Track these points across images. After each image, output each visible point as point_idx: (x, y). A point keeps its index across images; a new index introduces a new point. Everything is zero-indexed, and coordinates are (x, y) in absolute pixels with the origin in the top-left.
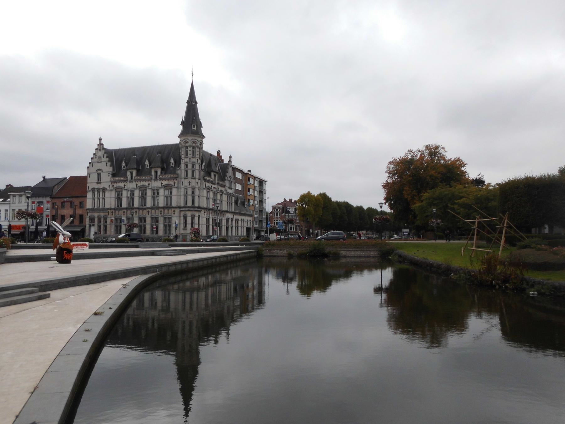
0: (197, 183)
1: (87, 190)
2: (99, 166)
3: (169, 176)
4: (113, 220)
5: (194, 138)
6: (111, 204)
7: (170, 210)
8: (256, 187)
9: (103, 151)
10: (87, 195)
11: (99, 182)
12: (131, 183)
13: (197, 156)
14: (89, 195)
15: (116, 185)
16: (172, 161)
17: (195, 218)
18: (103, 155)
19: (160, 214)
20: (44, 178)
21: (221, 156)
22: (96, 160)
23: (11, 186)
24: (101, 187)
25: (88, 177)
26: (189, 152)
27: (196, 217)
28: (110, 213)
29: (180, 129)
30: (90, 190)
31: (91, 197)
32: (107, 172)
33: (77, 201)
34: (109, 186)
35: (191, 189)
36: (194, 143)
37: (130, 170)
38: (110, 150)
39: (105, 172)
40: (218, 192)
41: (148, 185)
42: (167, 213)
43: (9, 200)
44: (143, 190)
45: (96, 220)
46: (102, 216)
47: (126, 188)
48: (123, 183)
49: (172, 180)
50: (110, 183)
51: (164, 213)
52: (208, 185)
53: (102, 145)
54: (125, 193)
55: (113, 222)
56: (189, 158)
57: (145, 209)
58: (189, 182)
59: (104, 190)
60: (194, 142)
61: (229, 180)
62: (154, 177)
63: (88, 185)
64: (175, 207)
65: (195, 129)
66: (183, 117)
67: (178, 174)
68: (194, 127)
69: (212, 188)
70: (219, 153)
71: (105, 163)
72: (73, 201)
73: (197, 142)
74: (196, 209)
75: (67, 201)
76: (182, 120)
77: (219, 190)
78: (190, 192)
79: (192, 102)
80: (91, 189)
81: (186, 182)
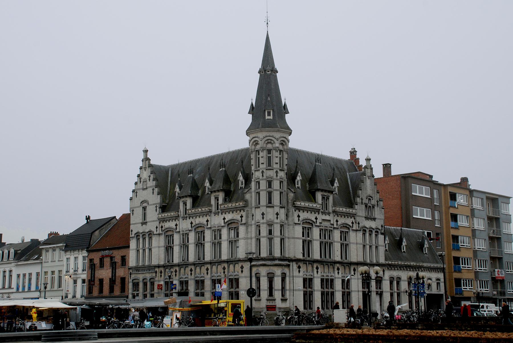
0: (277, 214)
1: (130, 235)
2: (143, 195)
3: (234, 205)
4: (162, 285)
5: (268, 135)
6: (159, 259)
7: (219, 266)
8: (476, 211)
9: (149, 170)
10: (130, 245)
11: (144, 223)
12: (185, 220)
13: (275, 166)
14: (133, 244)
15: (167, 225)
16: (241, 178)
17: (275, 278)
18: (149, 177)
19: (223, 273)
20: (88, 218)
21: (358, 159)
22: (140, 186)
23: (57, 234)
24: (147, 231)
25: (131, 214)
26: (261, 160)
27: (278, 276)
28: (158, 274)
29: (249, 119)
32: (154, 204)
33: (117, 255)
34: (157, 228)
35: (265, 225)
36: (268, 143)
37: (183, 199)
38: (164, 167)
39: (151, 205)
40: (334, 228)
41: (206, 223)
42: (233, 271)
43: (41, 258)
44: (199, 230)
45: (141, 285)
46: (148, 279)
47: (178, 230)
49: (238, 212)
50: (158, 222)
51: (228, 272)
52: (304, 215)
53: (149, 160)
54: (177, 239)
55: (161, 289)
57: (172, 266)
58: (263, 214)
59: (150, 234)
60: (269, 141)
61: (367, 202)
62: (214, 209)
63: (132, 227)
64: (243, 260)
65: (271, 117)
67: (246, 201)
68: (269, 114)
69: (318, 221)
70: (353, 153)
71: (150, 190)
72: (114, 256)
73: (273, 139)
74: (277, 262)
75: (107, 256)
76: (252, 104)
78: (264, 232)
79: (265, 71)
80: (135, 234)
81: (258, 213)
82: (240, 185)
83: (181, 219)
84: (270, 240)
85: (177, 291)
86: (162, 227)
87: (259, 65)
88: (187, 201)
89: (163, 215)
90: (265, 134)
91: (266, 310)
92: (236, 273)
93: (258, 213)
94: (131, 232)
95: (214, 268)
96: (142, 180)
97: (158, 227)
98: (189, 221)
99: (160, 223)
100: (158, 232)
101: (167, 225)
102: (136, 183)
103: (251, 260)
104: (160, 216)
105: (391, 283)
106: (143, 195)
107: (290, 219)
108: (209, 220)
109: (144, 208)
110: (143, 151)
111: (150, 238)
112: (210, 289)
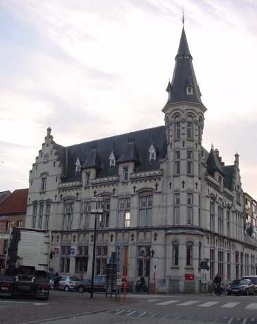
11: (43, 192)
12: (125, 185)
14: (30, 211)
15: (66, 194)
18: (51, 152)
35: (185, 194)
39: (51, 176)
53: (52, 137)
56: (182, 141)
57: (107, 231)
58: (183, 183)
59: (49, 202)
62: (122, 179)
68: (190, 91)
82: (151, 158)
84: (41, 217)
85: (75, 255)
86: (61, 196)
87: (175, 52)
89: (64, 185)
90: (186, 107)
91: (184, 278)
92: (125, 241)
93: (177, 184)
95: (82, 235)
96: (43, 155)
98: (91, 191)
99: (59, 192)
101: (66, 194)
102: (37, 158)
103: (166, 229)
104: (60, 185)
105: (237, 256)
106: (43, 168)
107: (203, 191)
108: (116, 189)
109: (44, 179)
111: (48, 206)
112: (134, 256)
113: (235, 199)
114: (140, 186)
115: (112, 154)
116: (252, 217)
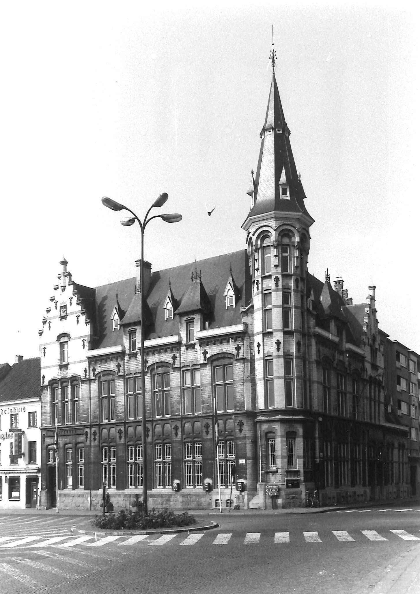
9: (70, 289)
11: (64, 367)
15: (100, 368)
18: (71, 299)
30: (46, 383)
31: (262, 377)
32: (80, 338)
34: (85, 371)
39: (74, 339)
48: (114, 359)
56: (273, 277)
59: (74, 381)
60: (286, 232)
63: (43, 372)
66: (252, 173)
73: (292, 229)
77: (352, 367)
82: (228, 304)
83: (183, 348)
88: (136, 330)
94: (42, 379)
96: (59, 305)
97: (88, 369)
100: (88, 377)
108: (122, 364)
110: (61, 263)
111: (74, 388)
113: (368, 358)
114: (213, 350)
115: (229, 287)
116: (409, 381)
